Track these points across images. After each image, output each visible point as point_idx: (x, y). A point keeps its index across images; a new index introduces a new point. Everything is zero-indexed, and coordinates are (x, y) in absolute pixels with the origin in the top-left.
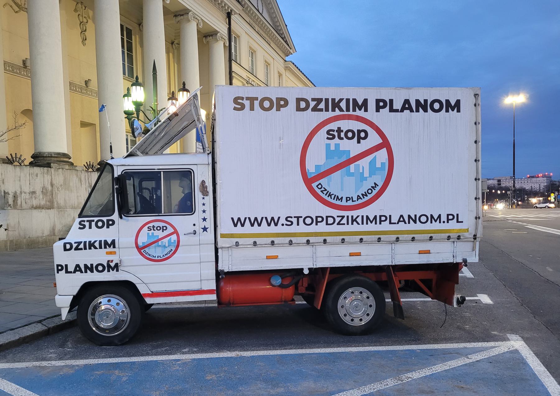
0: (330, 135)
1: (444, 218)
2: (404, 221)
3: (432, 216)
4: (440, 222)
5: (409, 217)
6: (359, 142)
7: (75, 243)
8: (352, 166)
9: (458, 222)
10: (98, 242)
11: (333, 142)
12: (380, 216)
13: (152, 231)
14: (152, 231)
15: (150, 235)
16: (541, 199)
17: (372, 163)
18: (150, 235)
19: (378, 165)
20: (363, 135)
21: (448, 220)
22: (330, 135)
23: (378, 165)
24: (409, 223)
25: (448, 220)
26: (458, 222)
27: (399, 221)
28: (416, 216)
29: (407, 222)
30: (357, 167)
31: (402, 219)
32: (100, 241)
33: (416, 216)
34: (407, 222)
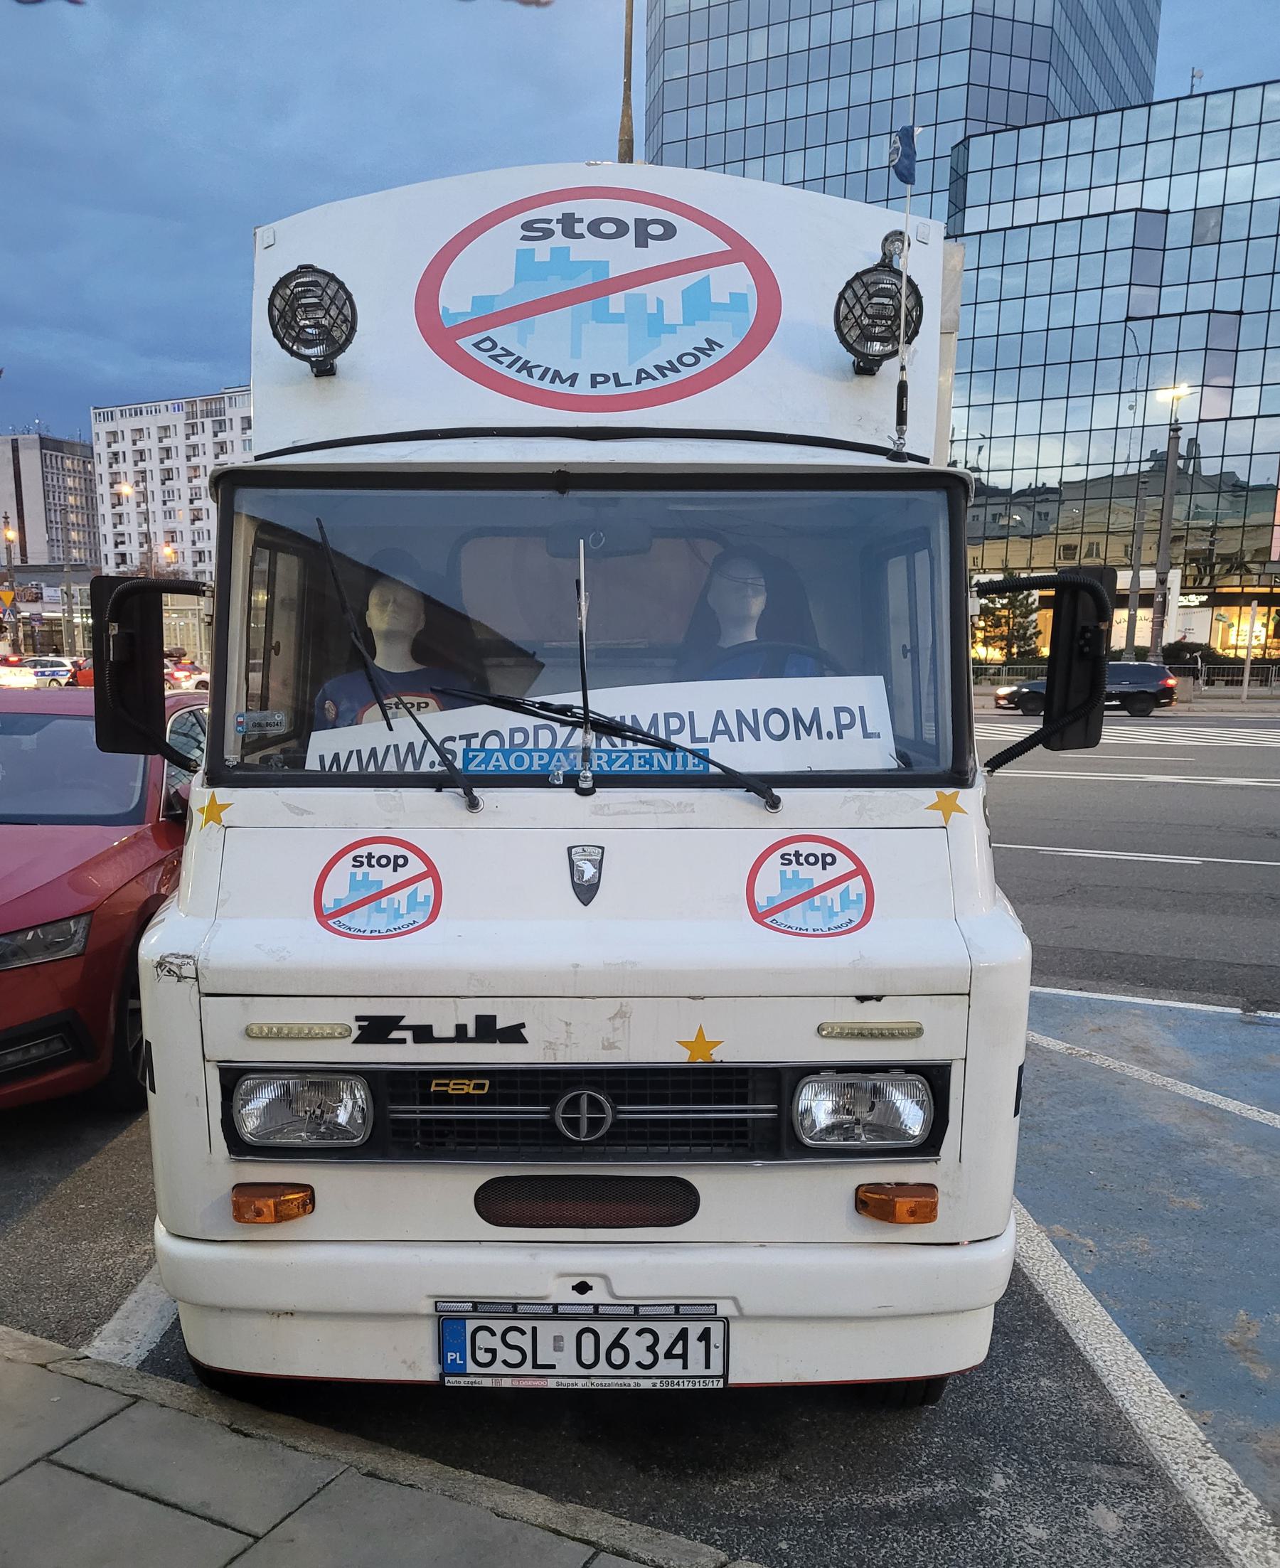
0: (358, 862)
1: (828, 723)
2: (727, 731)
3: (798, 718)
4: (820, 737)
5: (740, 716)
6: (824, 868)
7: (502, 349)
8: (817, 898)
9: (867, 735)
10: (541, 370)
11: (789, 870)
12: (668, 716)
13: (365, 868)
14: (365, 868)
15: (359, 878)
16: (1204, 598)
17: (844, 895)
18: (359, 878)
19: (853, 897)
20: (401, 861)
21: (841, 728)
22: (358, 862)
23: (853, 897)
24: (741, 739)
25: (841, 728)
26: (867, 735)
27: (715, 732)
28: (755, 712)
29: (736, 737)
30: (824, 899)
31: (721, 727)
32: (547, 370)
33: (755, 712)
34: (736, 737)
